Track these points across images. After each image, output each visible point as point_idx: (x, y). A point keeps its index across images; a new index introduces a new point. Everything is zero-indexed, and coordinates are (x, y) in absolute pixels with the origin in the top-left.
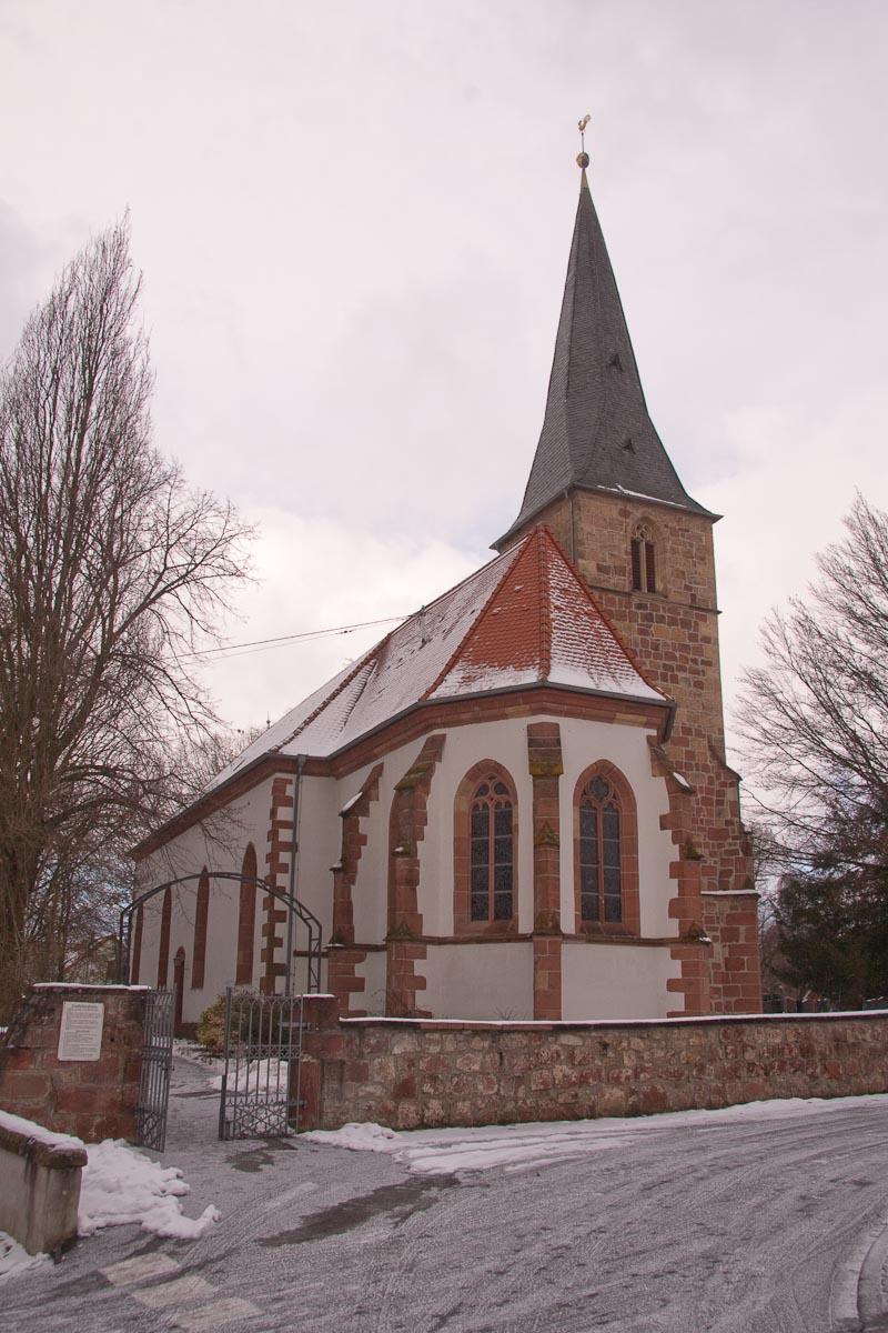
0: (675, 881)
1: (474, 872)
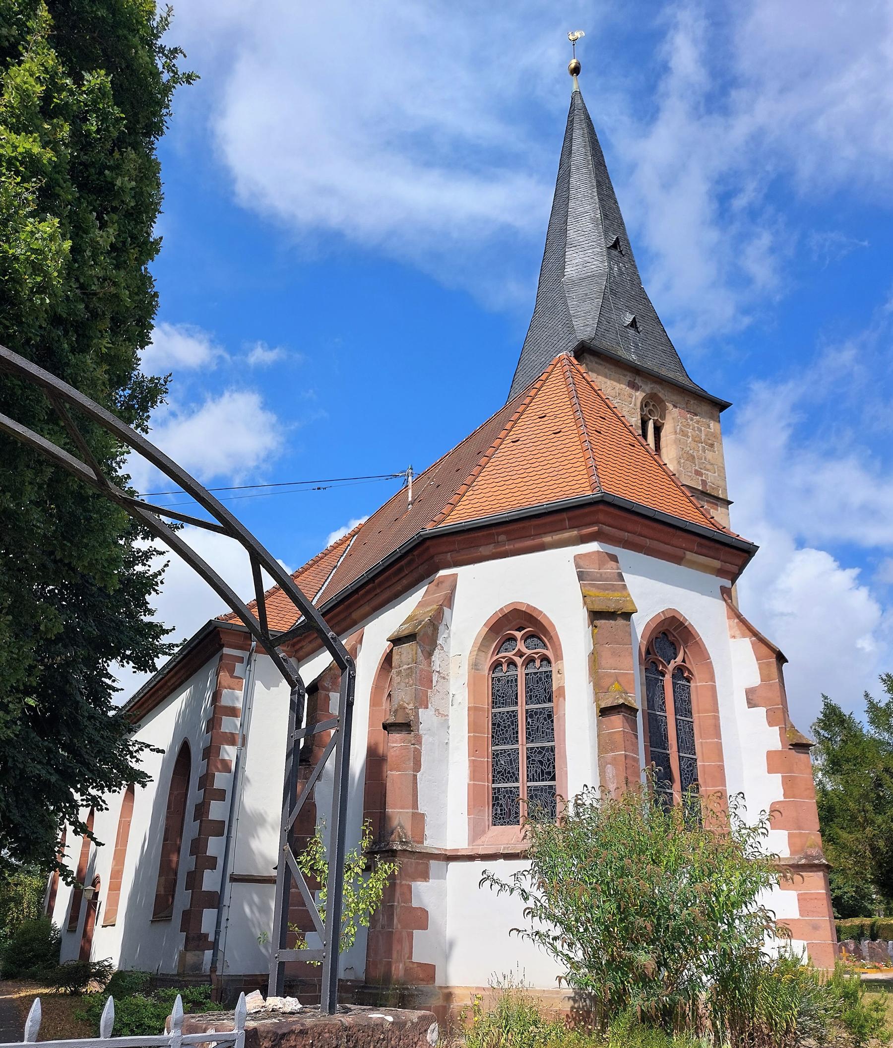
0: (778, 778)
1: (495, 755)
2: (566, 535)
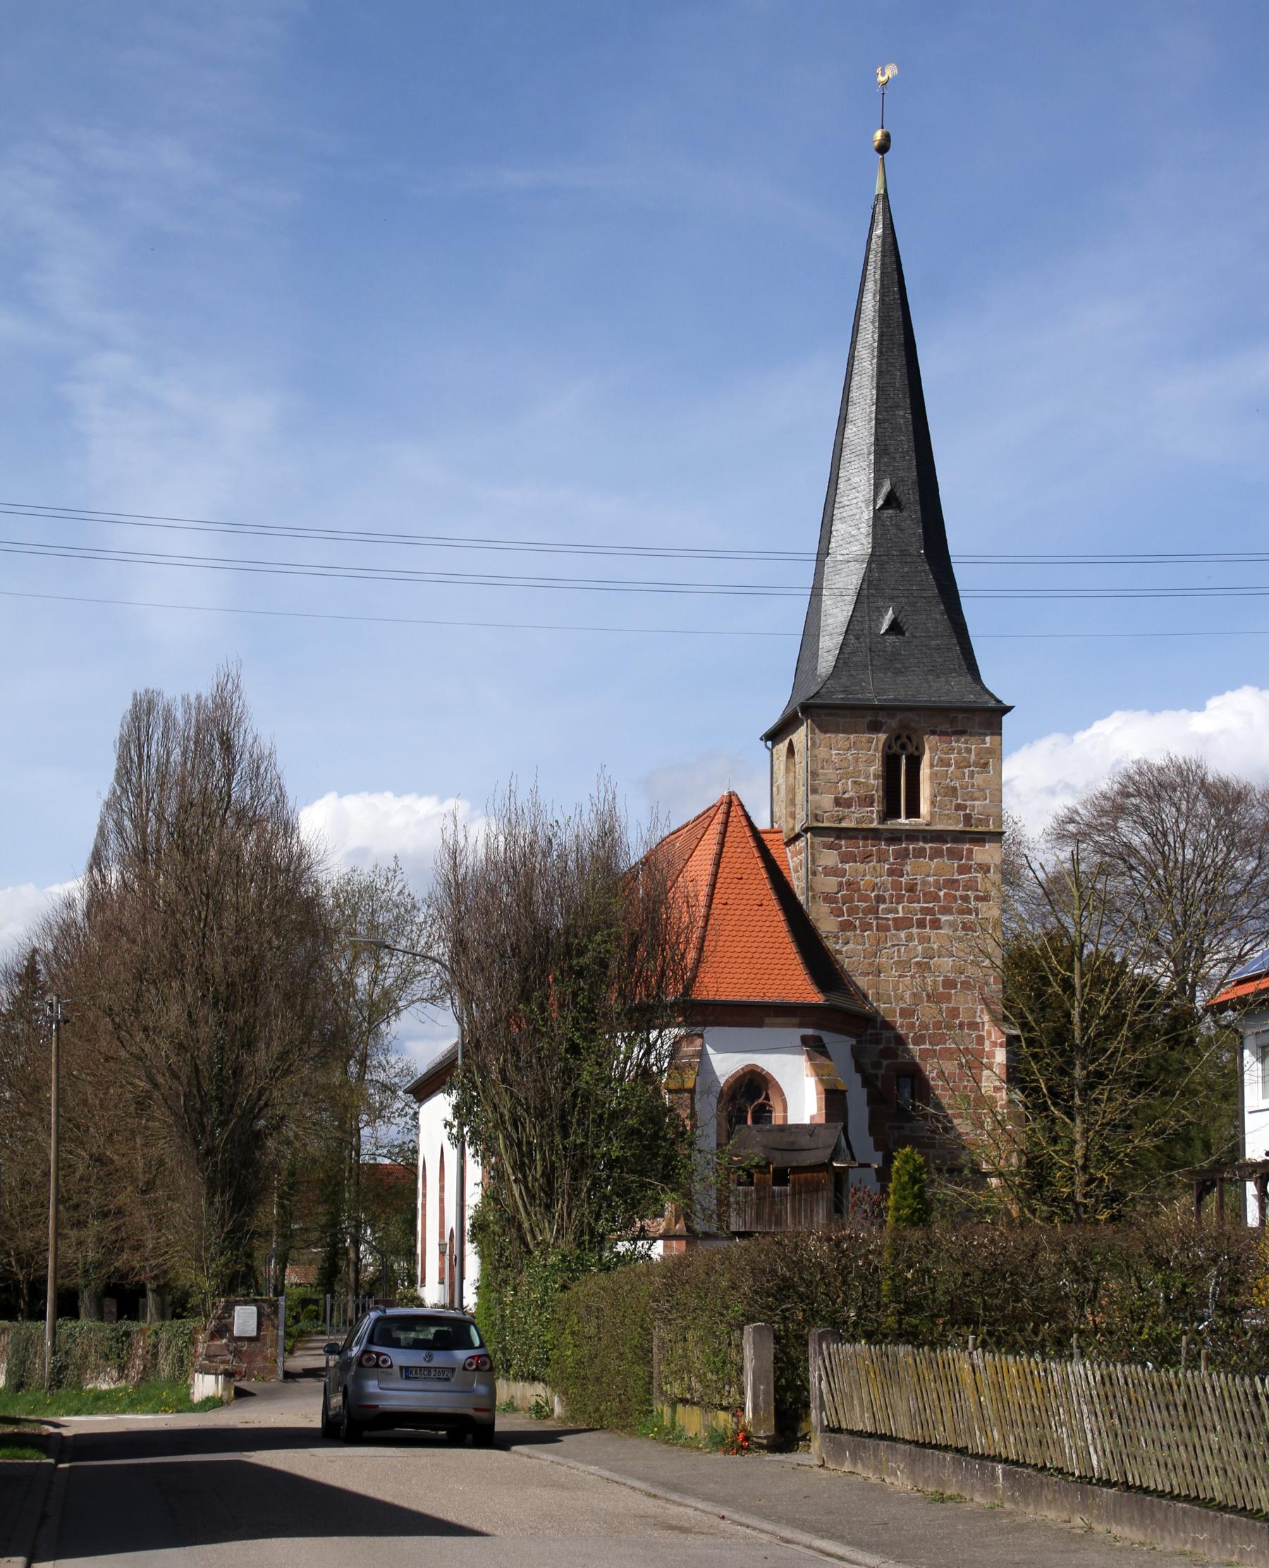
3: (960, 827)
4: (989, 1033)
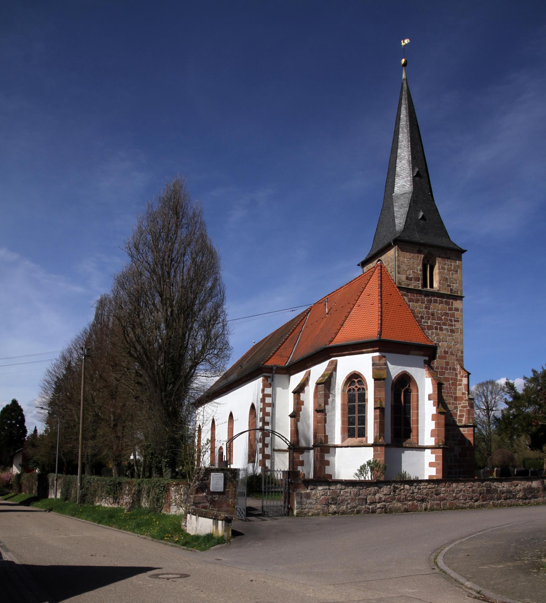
1: (349, 418)
2: (369, 350)
3: (449, 293)
4: (460, 373)
